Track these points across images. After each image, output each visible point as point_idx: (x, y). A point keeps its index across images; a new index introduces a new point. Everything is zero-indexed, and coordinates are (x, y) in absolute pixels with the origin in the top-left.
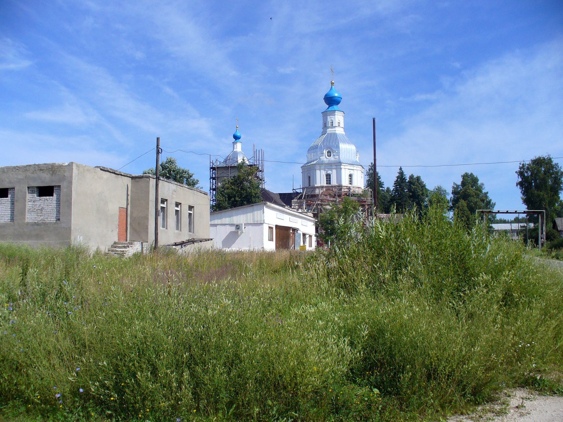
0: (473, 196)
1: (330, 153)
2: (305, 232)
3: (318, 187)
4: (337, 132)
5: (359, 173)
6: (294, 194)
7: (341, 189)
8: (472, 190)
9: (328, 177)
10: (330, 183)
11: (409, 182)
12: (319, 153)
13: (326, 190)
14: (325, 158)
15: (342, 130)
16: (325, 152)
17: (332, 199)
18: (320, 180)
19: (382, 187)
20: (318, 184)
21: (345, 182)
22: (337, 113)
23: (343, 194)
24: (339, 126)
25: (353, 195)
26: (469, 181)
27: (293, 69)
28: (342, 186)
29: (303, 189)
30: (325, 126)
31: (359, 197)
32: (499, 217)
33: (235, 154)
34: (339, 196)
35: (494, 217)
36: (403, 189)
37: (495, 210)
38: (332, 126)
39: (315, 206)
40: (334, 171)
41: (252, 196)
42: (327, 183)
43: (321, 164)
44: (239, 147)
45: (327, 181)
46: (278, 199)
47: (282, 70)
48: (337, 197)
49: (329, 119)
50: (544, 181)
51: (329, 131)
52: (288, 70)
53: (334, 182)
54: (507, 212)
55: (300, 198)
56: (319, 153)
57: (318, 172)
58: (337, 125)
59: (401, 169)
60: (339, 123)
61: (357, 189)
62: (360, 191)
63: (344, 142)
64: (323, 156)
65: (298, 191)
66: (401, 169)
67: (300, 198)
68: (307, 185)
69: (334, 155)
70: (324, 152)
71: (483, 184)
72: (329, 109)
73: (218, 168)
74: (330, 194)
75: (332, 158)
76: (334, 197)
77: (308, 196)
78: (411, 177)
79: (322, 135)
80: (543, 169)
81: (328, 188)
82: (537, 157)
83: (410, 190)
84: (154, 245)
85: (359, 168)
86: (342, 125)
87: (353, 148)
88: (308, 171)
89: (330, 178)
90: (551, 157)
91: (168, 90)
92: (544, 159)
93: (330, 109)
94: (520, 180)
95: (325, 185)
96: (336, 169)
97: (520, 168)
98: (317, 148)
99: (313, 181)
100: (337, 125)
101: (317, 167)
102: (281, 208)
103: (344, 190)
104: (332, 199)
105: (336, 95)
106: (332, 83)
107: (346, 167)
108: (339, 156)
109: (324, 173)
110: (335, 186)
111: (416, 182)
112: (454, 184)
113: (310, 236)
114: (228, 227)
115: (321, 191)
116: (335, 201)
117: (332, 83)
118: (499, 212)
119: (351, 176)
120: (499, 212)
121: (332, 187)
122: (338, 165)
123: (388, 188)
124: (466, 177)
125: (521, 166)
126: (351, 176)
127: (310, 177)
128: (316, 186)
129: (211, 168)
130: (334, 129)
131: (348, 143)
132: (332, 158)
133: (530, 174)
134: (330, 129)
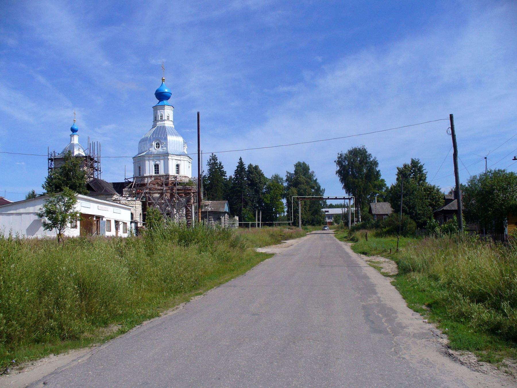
0: (303, 184)
1: (159, 144)
2: (118, 219)
3: (147, 177)
4: (166, 125)
5: (186, 163)
6: (126, 183)
7: (168, 179)
8: (302, 178)
9: (157, 166)
10: (158, 173)
11: (247, 171)
12: (148, 144)
13: (155, 179)
14: (154, 150)
15: (172, 123)
16: (154, 144)
17: (159, 188)
18: (149, 170)
19: (225, 176)
20: (147, 174)
21: (172, 172)
22: (166, 107)
23: (170, 183)
24: (168, 119)
25: (180, 184)
26: (302, 169)
27: (164, 60)
28: (169, 176)
29: (134, 178)
30: (156, 120)
31: (185, 185)
32: (329, 202)
33: (72, 146)
34: (167, 185)
35: (325, 202)
36: (242, 178)
37: (325, 196)
38: (162, 120)
39: (143, 195)
40: (162, 162)
41: (76, 186)
42: (155, 173)
43: (150, 156)
44: (76, 140)
45: (155, 171)
46: (112, 189)
47: (153, 62)
48: (164, 185)
49: (159, 113)
50: (360, 170)
51: (159, 124)
52: (159, 61)
53: (162, 172)
54: (336, 198)
55: (131, 187)
56: (148, 144)
57: (147, 162)
58: (166, 118)
59: (241, 159)
60: (168, 117)
61: (184, 178)
62: (187, 180)
63: (172, 134)
64: (151, 147)
65: (130, 180)
66: (241, 159)
67: (131, 187)
68: (137, 175)
69: (162, 147)
70: (153, 144)
71: (313, 172)
72: (160, 104)
73: (55, 159)
74: (158, 183)
75: (160, 150)
76: (161, 186)
77: (138, 185)
78: (250, 166)
79: (153, 128)
80: (359, 159)
81: (156, 178)
82: (354, 148)
83: (248, 179)
84: (369, 263)
85: (186, 158)
86: (171, 118)
87: (180, 139)
88: (139, 162)
89: (158, 168)
90: (365, 147)
91: (41, 79)
92: (360, 149)
93: (161, 103)
94: (338, 168)
95: (154, 174)
96: (164, 159)
97: (339, 158)
98: (147, 140)
99: (143, 171)
100: (166, 118)
101: (147, 158)
102: (85, 197)
103: (171, 179)
104: (159, 188)
105: (166, 90)
106: (163, 80)
107: (173, 158)
108: (167, 147)
109: (152, 163)
110: (162, 176)
111: (254, 170)
112: (288, 173)
113: (125, 224)
114: (32, 215)
115: (150, 181)
116: (162, 190)
117: (163, 80)
118: (328, 198)
119: (178, 166)
120: (328, 198)
121: (160, 176)
122: (165, 155)
123: (231, 177)
124: (415, 164)
125: (339, 156)
126: (178, 166)
127: (140, 168)
128: (145, 175)
129: (49, 159)
130: (163, 122)
131: (176, 135)
132: (160, 150)
133: (347, 163)
134: (160, 123)
